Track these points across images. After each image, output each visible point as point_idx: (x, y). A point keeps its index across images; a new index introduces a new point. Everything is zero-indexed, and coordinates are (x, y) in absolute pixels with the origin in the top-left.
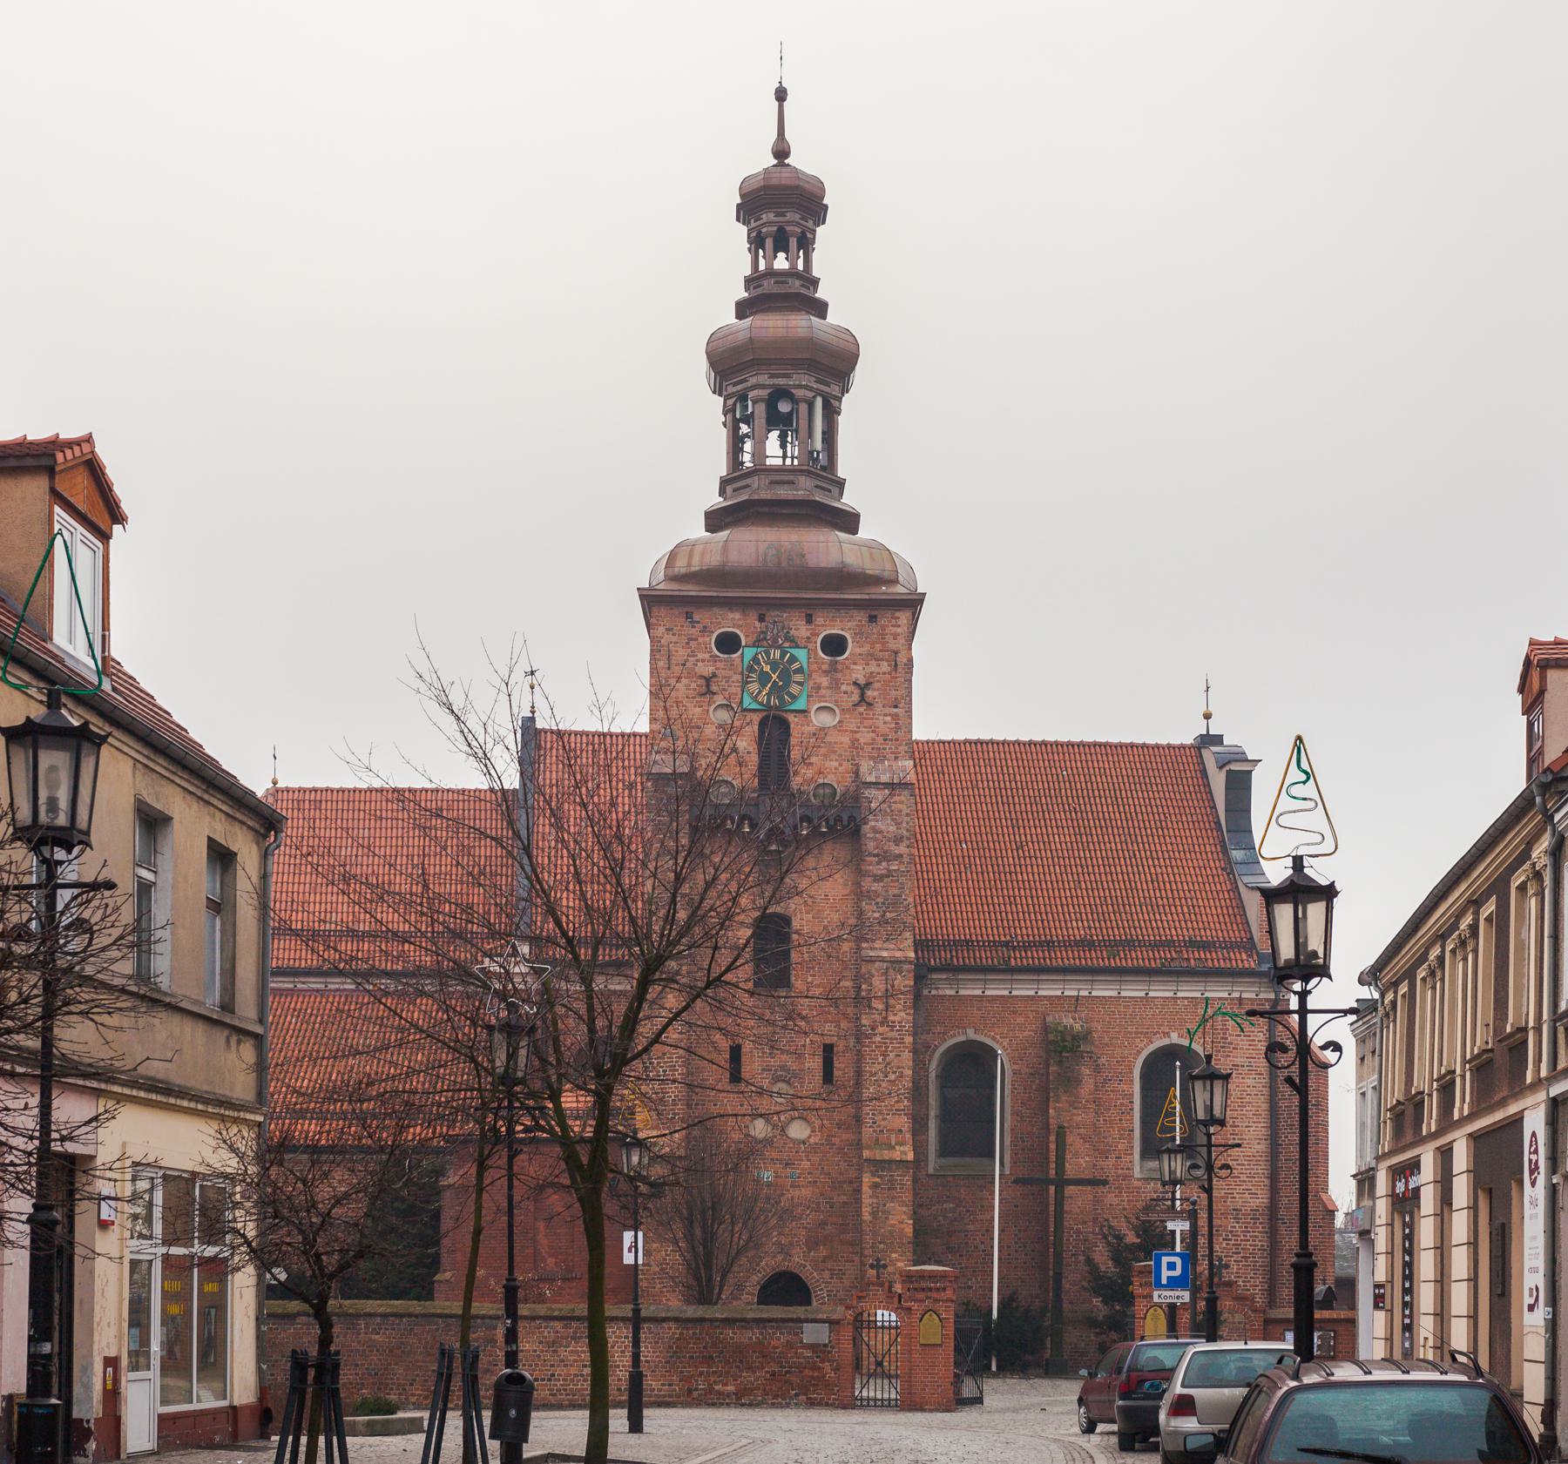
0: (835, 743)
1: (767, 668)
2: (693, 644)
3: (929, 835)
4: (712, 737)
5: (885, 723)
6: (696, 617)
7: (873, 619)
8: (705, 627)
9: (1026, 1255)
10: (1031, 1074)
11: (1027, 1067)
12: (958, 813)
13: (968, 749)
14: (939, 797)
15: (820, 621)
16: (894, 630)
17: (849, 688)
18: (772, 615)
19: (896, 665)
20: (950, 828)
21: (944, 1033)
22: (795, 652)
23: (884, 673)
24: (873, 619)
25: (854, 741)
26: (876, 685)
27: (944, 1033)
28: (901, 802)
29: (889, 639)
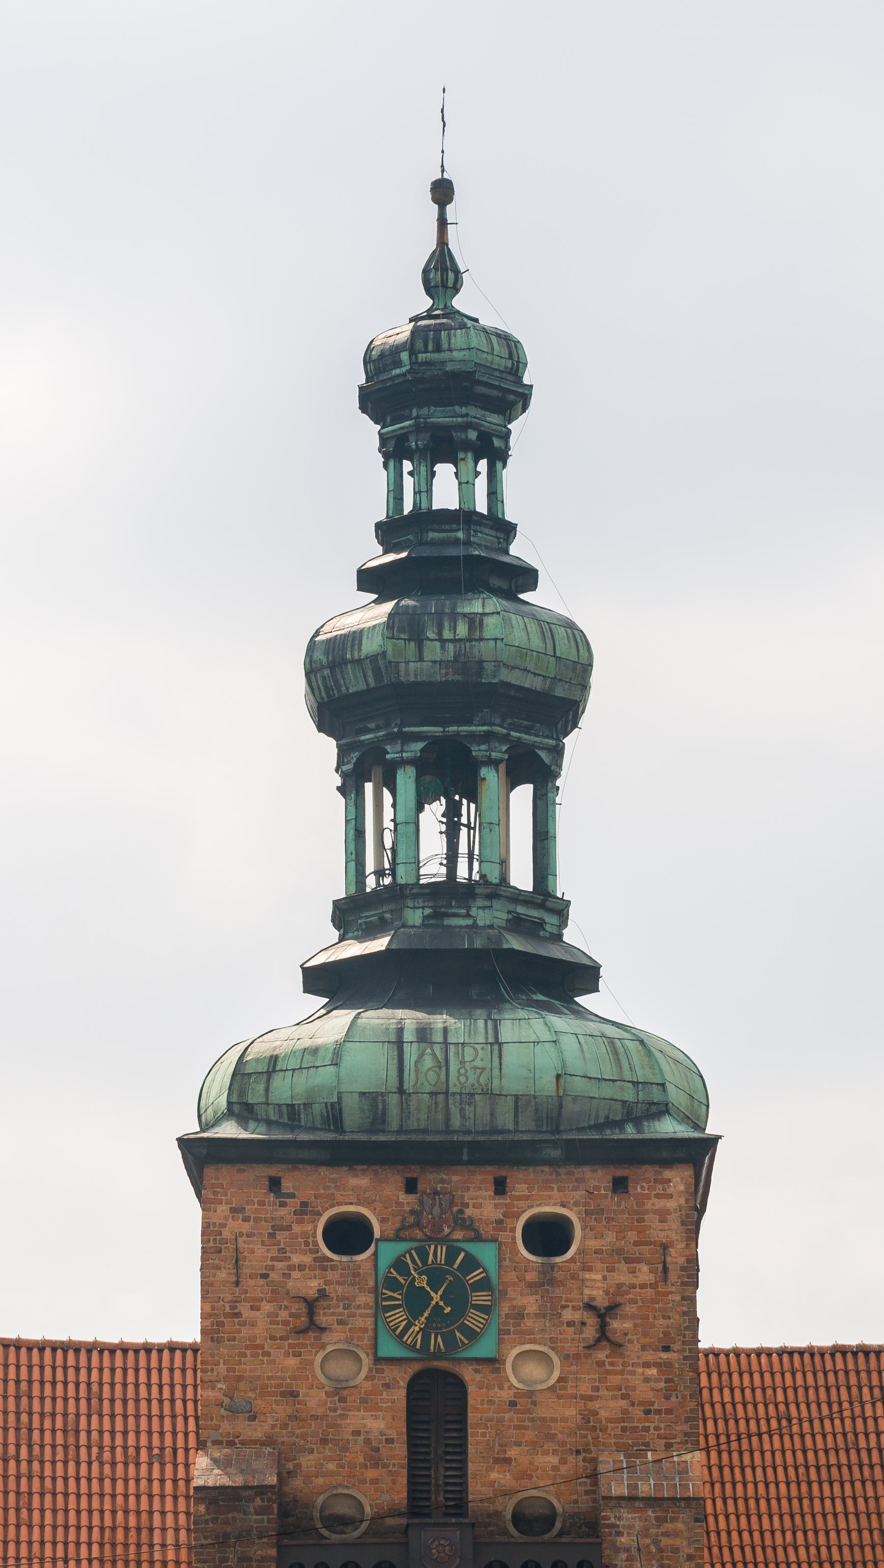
0: (554, 1420)
1: (422, 1282)
2: (281, 1236)
3: (759, 1550)
4: (320, 1411)
5: (647, 1380)
6: (287, 1185)
7: (620, 1185)
8: (304, 1204)
12: (817, 1502)
13: (840, 1365)
14: (780, 1470)
15: (521, 1189)
16: (661, 1204)
17: (577, 1316)
18: (429, 1180)
19: (665, 1270)
20: (800, 1535)
22: (474, 1248)
23: (643, 1286)
25: (588, 1419)
26: (629, 1309)
28: (676, 1534)
29: (651, 1220)
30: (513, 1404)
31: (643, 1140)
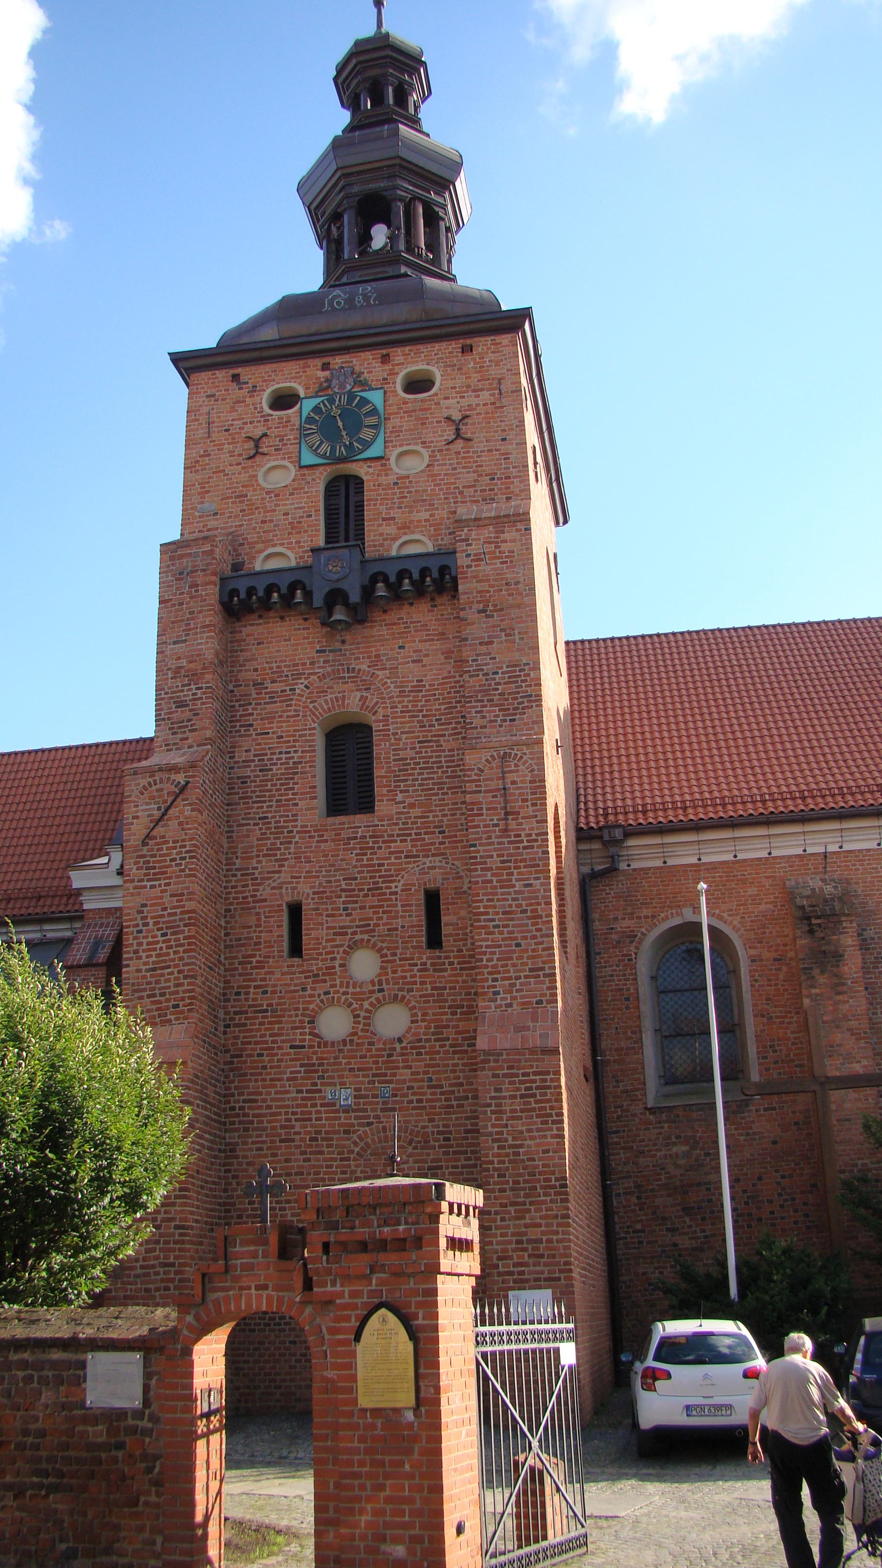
6: (243, 378)
9: (795, 1211)
10: (775, 960)
11: (769, 951)
15: (400, 359)
18: (337, 361)
21: (653, 917)
24: (467, 350)
27: (653, 917)
30: (396, 484)
31: (441, 1539)
